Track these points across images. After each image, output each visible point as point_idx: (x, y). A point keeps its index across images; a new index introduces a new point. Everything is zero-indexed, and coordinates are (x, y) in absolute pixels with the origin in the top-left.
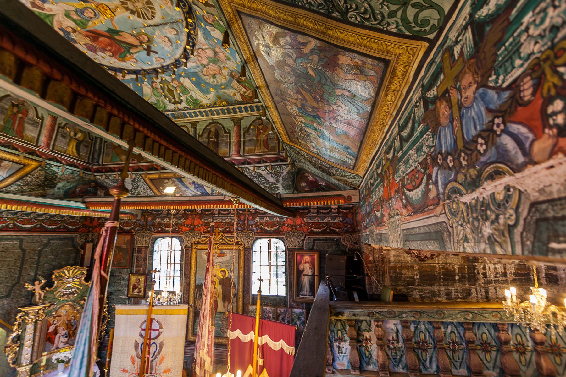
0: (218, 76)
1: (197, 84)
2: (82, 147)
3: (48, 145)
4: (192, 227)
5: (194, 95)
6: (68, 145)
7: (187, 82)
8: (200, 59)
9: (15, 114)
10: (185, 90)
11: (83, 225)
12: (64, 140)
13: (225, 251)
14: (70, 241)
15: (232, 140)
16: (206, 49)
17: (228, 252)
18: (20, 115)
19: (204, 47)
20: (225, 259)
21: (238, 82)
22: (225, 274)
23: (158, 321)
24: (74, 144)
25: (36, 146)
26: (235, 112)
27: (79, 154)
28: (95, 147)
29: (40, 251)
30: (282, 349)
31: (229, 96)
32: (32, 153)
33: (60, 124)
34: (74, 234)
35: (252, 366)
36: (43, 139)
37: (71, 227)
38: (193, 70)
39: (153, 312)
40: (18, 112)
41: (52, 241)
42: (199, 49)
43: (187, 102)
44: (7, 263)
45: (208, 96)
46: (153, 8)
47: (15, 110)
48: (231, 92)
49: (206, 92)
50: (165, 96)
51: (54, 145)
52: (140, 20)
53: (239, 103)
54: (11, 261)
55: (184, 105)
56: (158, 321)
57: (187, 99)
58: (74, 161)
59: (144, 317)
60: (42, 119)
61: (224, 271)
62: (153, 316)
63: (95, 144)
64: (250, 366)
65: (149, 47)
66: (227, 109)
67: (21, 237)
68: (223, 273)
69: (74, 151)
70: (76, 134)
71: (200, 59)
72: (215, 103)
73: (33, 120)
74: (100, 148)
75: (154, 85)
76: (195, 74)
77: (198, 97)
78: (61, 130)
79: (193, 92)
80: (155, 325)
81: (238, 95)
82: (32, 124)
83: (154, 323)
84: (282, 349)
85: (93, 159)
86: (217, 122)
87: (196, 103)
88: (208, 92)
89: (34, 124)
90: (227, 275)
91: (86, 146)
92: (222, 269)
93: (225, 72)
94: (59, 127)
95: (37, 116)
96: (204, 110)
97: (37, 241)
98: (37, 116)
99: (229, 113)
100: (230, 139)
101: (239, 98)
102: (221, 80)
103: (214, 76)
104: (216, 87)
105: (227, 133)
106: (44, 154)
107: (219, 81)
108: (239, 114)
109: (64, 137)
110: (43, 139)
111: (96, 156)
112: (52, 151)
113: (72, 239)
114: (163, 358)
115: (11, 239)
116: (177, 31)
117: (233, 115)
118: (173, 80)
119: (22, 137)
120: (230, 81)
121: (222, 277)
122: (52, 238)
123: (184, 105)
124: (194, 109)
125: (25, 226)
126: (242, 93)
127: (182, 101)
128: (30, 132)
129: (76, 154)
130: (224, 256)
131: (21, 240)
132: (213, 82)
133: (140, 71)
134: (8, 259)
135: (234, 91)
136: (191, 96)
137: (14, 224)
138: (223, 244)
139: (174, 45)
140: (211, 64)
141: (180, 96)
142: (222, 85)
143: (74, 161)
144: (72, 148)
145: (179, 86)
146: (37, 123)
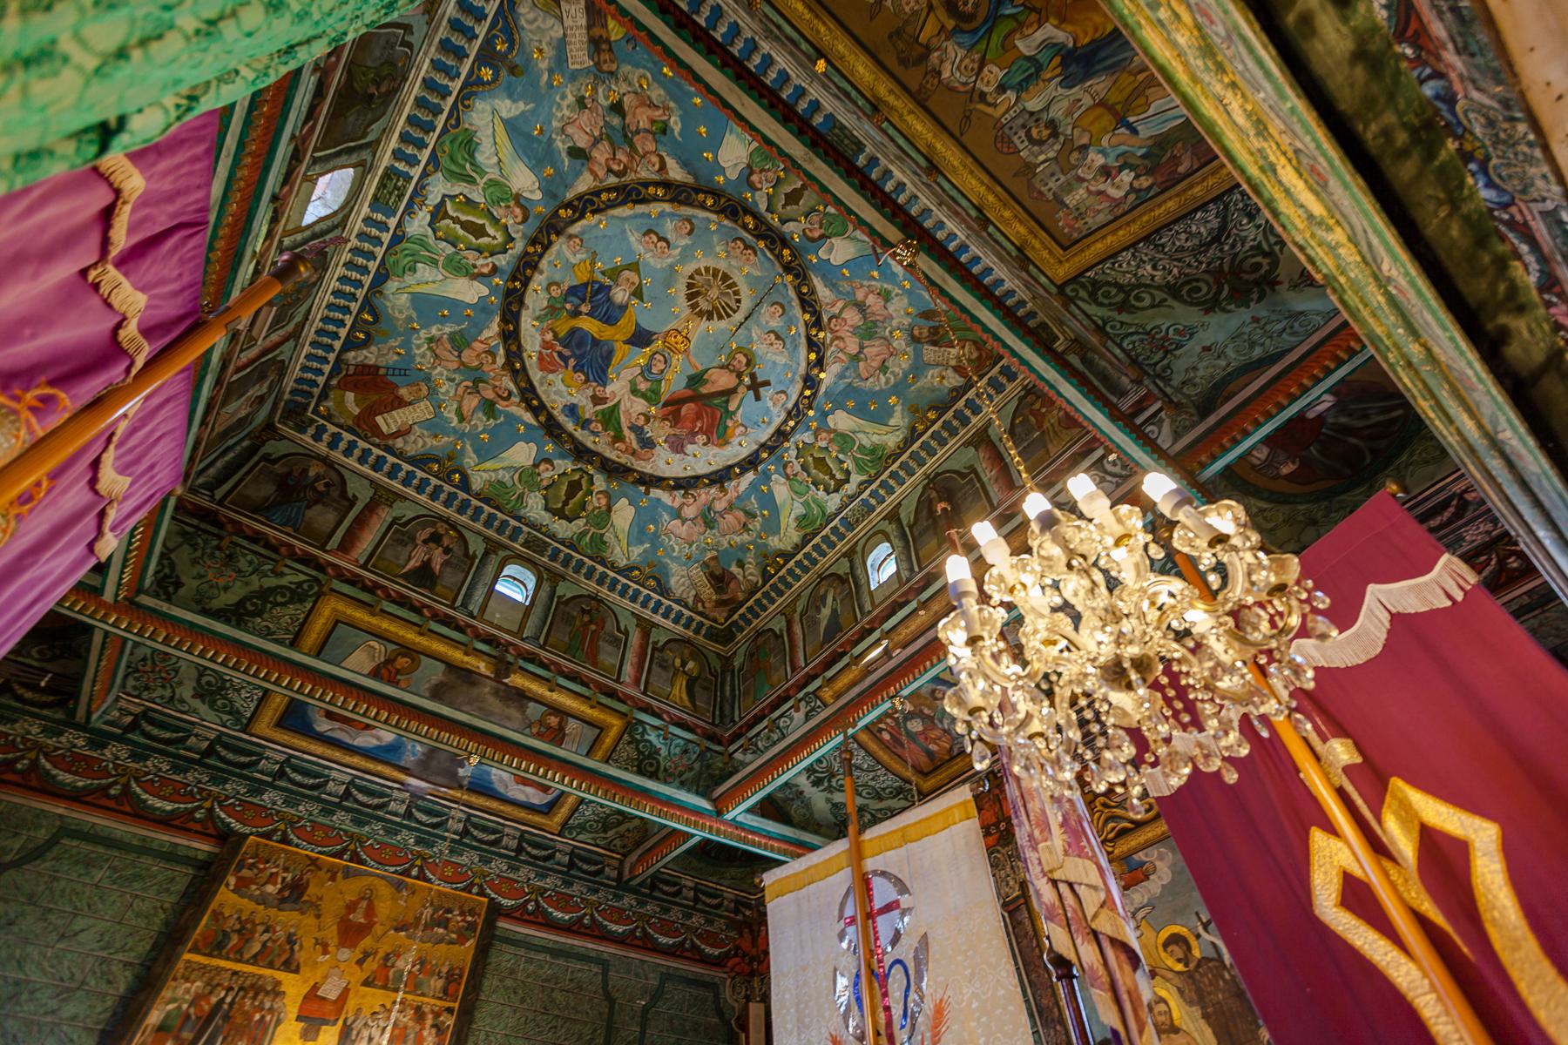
0: (889, 363)
1: (860, 411)
2: (698, 690)
3: (637, 682)
4: (1003, 826)
5: (866, 442)
6: (672, 685)
7: (842, 421)
8: (842, 345)
9: (586, 625)
10: (845, 440)
11: (737, 948)
12: (663, 673)
13: (1141, 856)
14: (710, 995)
15: (985, 479)
16: (841, 311)
17: (1154, 853)
18: (593, 627)
19: (836, 310)
20: (1154, 886)
21: (935, 343)
22: (1189, 948)
23: (883, 874)
24: (681, 683)
25: (618, 681)
26: (965, 422)
27: (694, 705)
28: (723, 692)
29: (645, 1009)
30: (1396, 618)
31: (933, 390)
32: (612, 694)
33: (656, 643)
34: (716, 974)
35: (1331, 829)
36: (628, 670)
37: (708, 950)
38: (842, 384)
39: (867, 849)
40: (591, 622)
41: (669, 986)
42: (830, 320)
43: (861, 470)
44: (578, 1027)
45: (892, 422)
46: (734, 284)
47: (586, 618)
48: (931, 377)
49: (881, 418)
50: (815, 484)
51: (647, 682)
52: (723, 324)
53: (959, 392)
54: (586, 1023)
55: (856, 478)
56: (883, 874)
57: (855, 460)
58: (685, 716)
59: (842, 879)
60: (626, 633)
61: (1175, 939)
62: (870, 864)
63: (723, 684)
64: (1318, 837)
65: (753, 376)
66: (946, 426)
67: (605, 956)
68: (1178, 951)
69: (684, 696)
70: (684, 664)
71: (842, 345)
72: (913, 429)
73: (612, 635)
74: (733, 691)
75: (789, 471)
76: (850, 390)
77: (875, 438)
78: (657, 654)
79: (860, 436)
80: (883, 892)
81: (950, 373)
82: (610, 643)
83: (878, 884)
84: (1399, 621)
85: (722, 716)
86: (938, 475)
87: (879, 458)
88: (889, 412)
89: (615, 642)
90: (1197, 953)
91: (705, 688)
92: (1164, 934)
93: (899, 341)
94: (654, 649)
95: (619, 630)
96: (898, 463)
97: (637, 975)
98: (619, 630)
99: (953, 432)
100: (979, 479)
101: (954, 380)
102: (900, 365)
103: (883, 368)
104: (899, 389)
105: (967, 475)
106: (632, 698)
107: (897, 370)
108: (974, 420)
109: (664, 668)
110: (628, 670)
111: (727, 711)
112: (644, 693)
113: (712, 987)
114: (939, 1012)
115: (584, 958)
116: (782, 306)
117: (965, 433)
118: (816, 434)
119: (595, 664)
120: (918, 355)
121: (1180, 967)
122: (666, 977)
123: (856, 478)
124: (878, 475)
125: (614, 927)
126: (953, 363)
127: (848, 473)
128: (608, 657)
129: (688, 704)
130: (1147, 878)
131: (604, 964)
132: (887, 382)
133: (757, 452)
134: (579, 1017)
135: (936, 371)
136: (861, 447)
137: (593, 918)
138: (1123, 833)
139: (788, 342)
140: (866, 343)
141: (842, 462)
142: (906, 375)
143: (685, 716)
144: (679, 690)
145: (831, 441)
146: (618, 640)
